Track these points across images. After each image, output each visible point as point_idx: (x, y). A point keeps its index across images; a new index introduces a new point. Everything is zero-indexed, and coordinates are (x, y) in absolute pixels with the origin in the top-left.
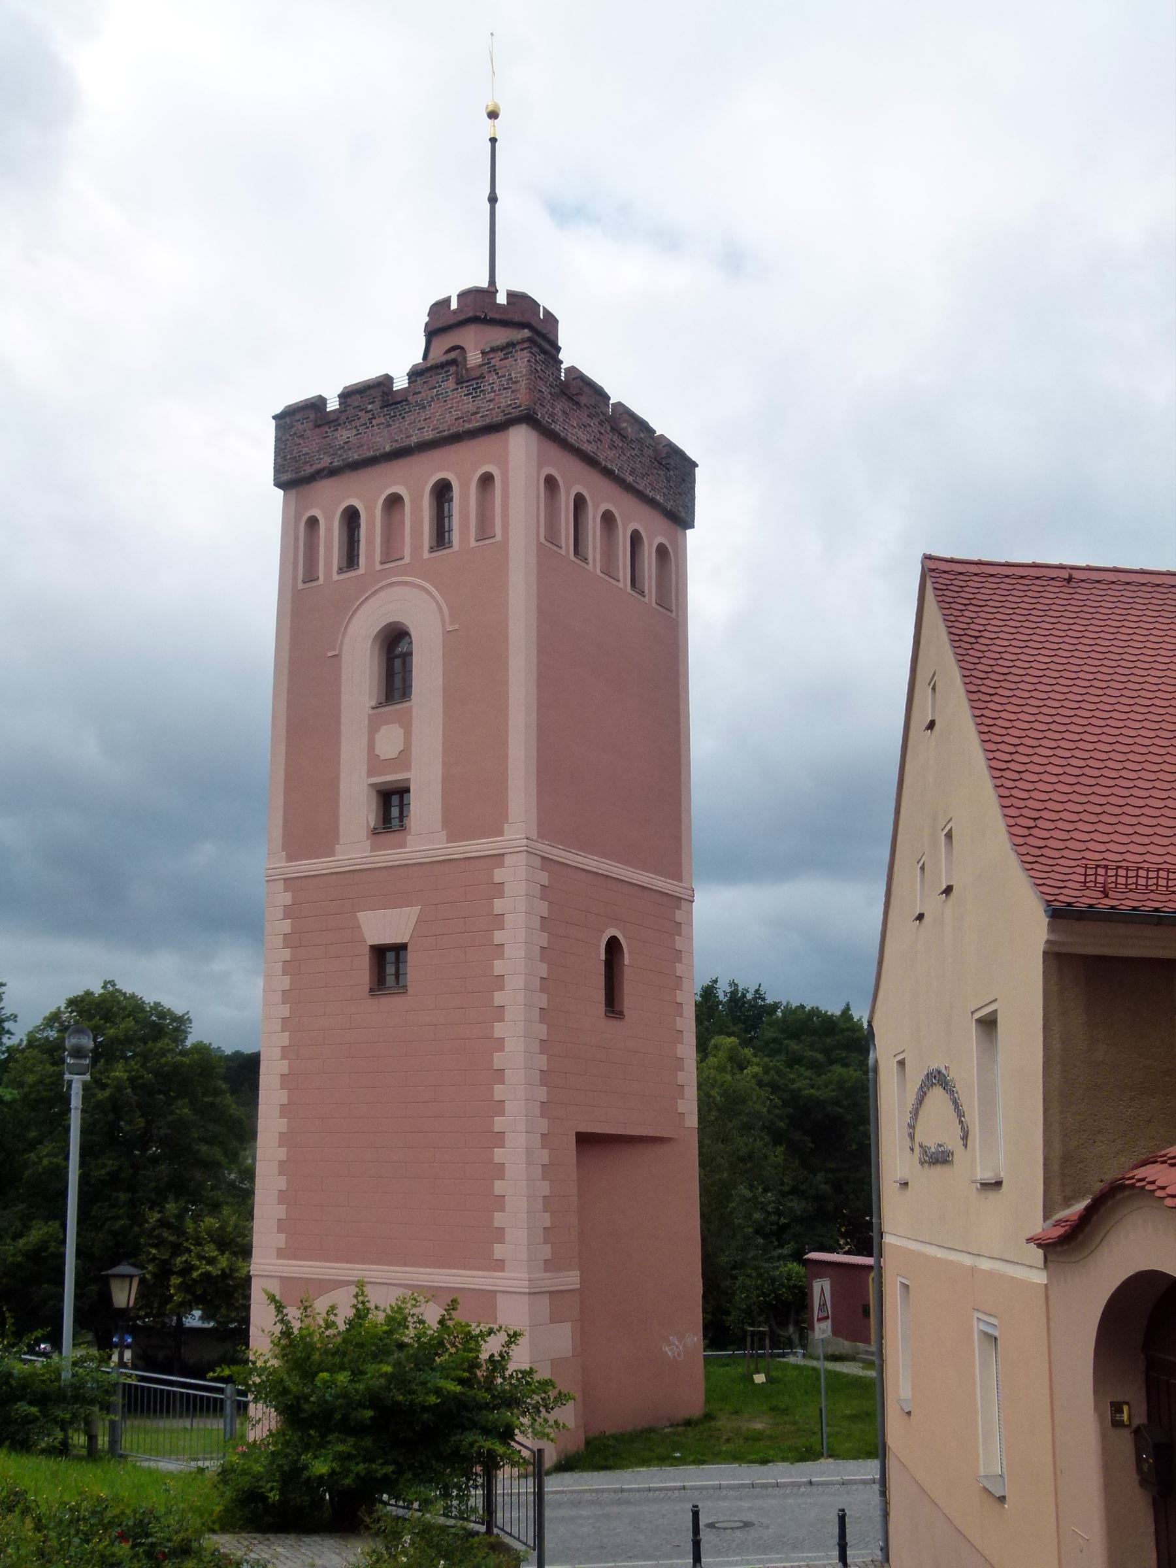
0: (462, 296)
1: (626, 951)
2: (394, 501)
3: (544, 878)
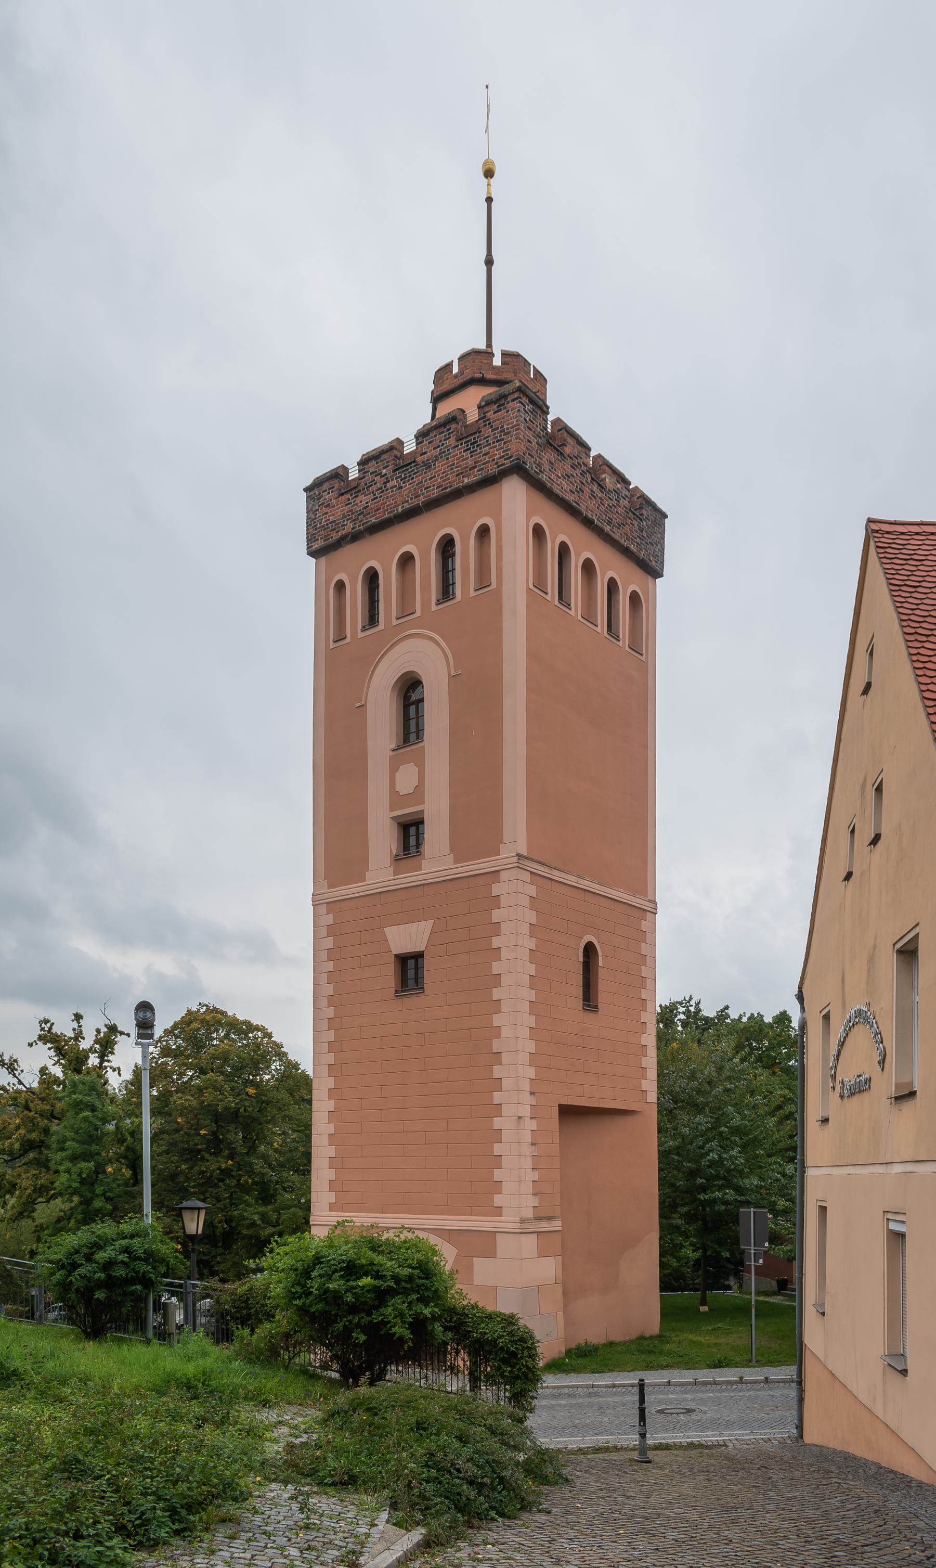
0: (462, 358)
1: (600, 954)
3: (532, 890)
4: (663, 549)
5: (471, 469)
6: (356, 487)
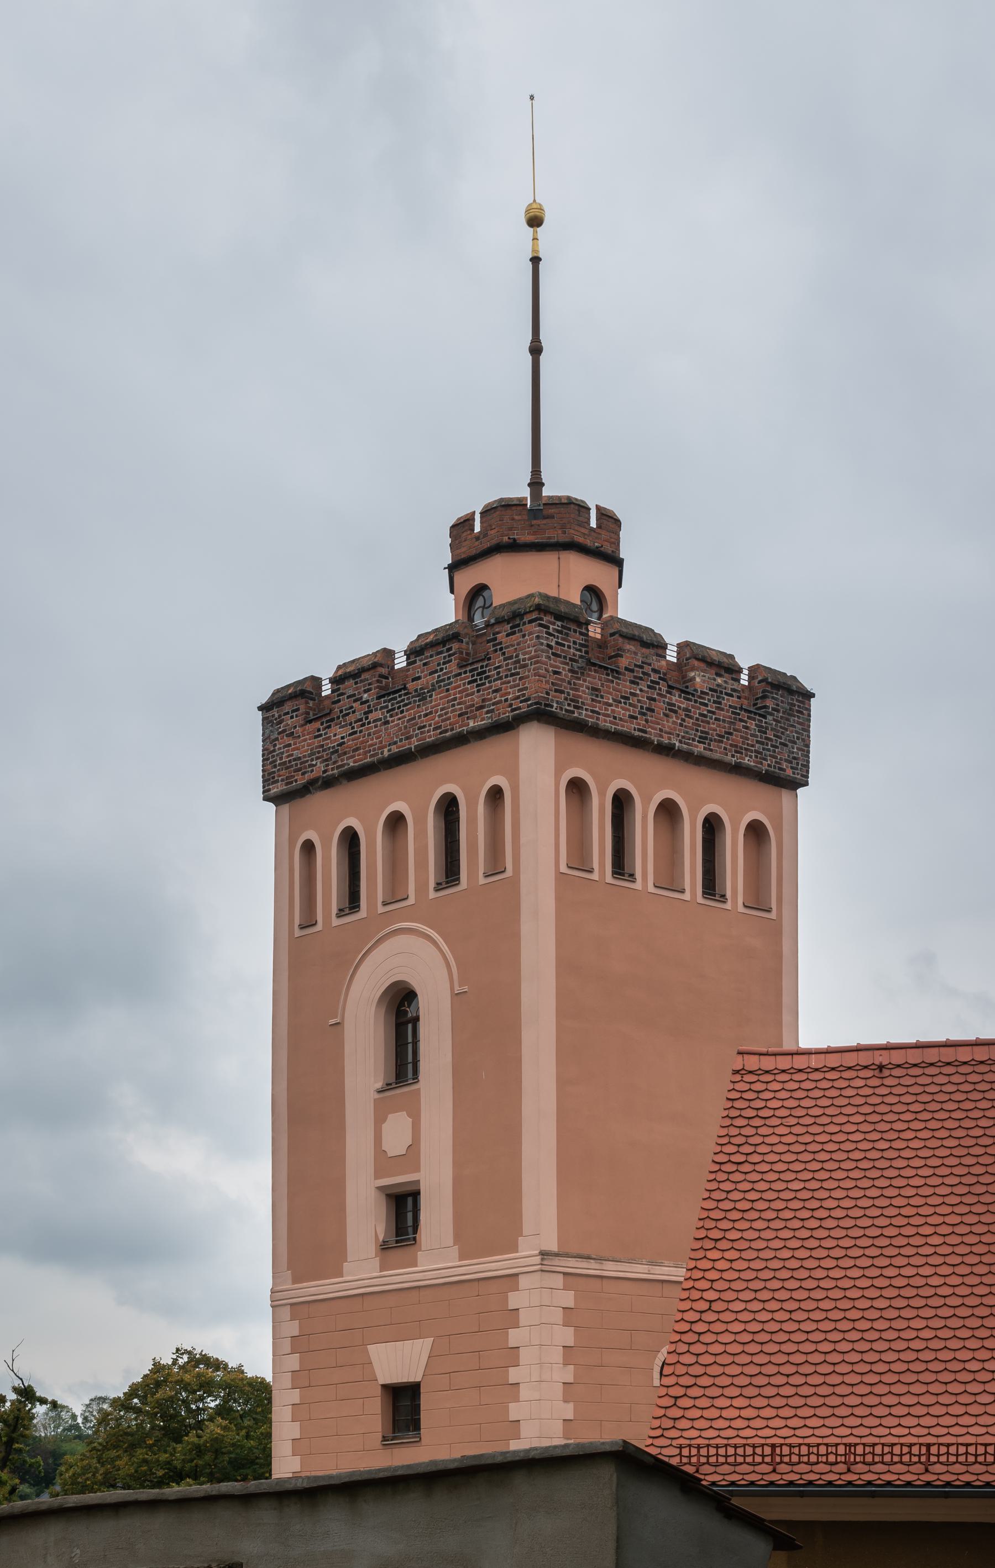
2: (396, 822)
3: (568, 1298)
4: (808, 746)
5: (478, 709)
6: (329, 714)
